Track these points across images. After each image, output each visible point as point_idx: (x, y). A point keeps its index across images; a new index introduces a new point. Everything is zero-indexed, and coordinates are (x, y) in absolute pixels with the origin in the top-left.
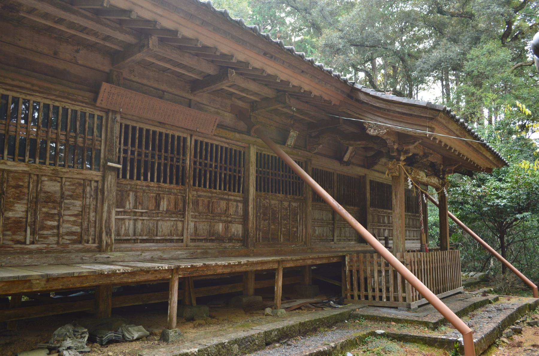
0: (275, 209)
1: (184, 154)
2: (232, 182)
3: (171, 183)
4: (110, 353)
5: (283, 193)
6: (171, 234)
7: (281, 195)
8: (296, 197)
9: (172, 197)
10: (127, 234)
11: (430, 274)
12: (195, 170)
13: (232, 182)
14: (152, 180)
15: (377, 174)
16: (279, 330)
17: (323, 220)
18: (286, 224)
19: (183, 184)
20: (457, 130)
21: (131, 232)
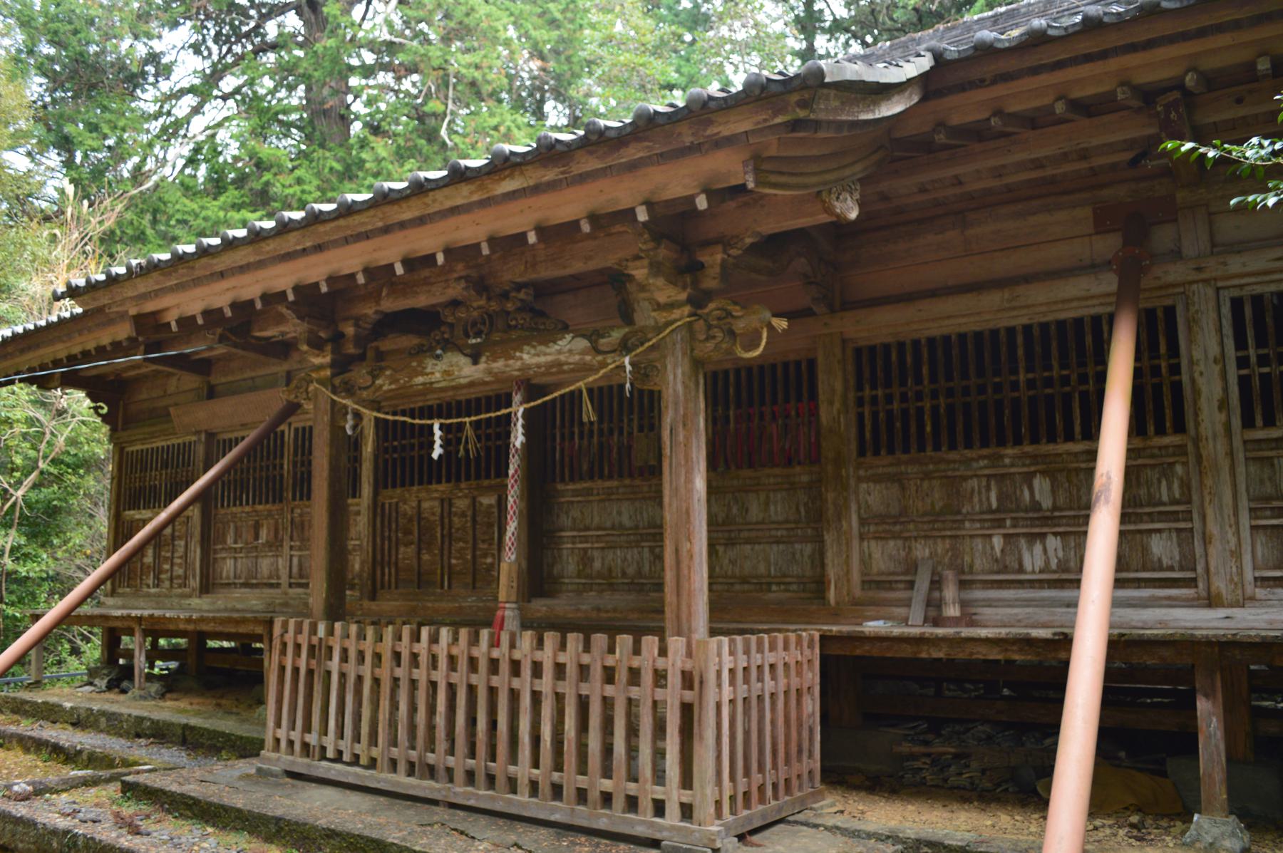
0: (432, 518)
1: (282, 456)
2: (960, 427)
3: (267, 502)
4: (780, 848)
5: (448, 481)
6: (270, 577)
7: (443, 487)
8: (486, 483)
9: (272, 522)
10: (228, 578)
11: (747, 733)
12: (295, 474)
13: (960, 427)
14: (247, 503)
15: (1096, 290)
16: (152, 721)
17: (621, 527)
18: (462, 548)
19: (281, 501)
20: (157, 283)
21: (232, 574)
